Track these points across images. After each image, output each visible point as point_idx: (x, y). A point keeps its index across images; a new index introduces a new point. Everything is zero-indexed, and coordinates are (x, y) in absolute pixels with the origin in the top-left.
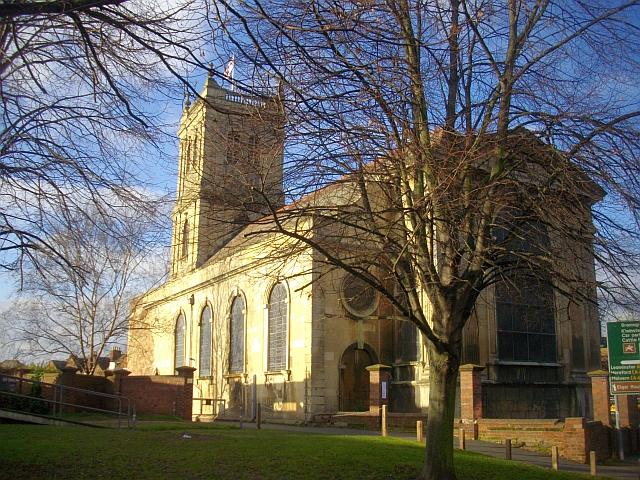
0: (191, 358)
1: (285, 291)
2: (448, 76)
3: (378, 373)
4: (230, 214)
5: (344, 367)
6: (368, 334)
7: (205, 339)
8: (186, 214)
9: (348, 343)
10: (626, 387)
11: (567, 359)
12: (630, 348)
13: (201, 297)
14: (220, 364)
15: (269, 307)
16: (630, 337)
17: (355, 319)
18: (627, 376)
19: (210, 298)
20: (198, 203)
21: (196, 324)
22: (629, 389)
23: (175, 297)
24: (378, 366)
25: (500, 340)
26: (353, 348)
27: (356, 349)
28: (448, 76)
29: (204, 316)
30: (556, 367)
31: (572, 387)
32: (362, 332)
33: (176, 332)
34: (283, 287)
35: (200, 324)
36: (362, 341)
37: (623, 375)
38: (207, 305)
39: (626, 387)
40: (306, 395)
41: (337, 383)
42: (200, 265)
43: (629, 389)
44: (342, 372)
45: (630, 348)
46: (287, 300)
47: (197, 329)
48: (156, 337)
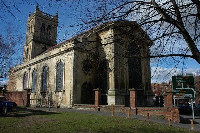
0: (29, 86)
1: (63, 64)
2: (176, 14)
3: (98, 91)
4: (42, 46)
5: (83, 89)
6: (90, 79)
7: (34, 81)
8: (28, 46)
9: (84, 82)
10: (178, 96)
11: (144, 89)
12: (179, 84)
13: (32, 67)
14: (144, 86)
15: (57, 70)
16: (179, 81)
17: (86, 74)
18: (178, 93)
19: (36, 67)
20: (32, 43)
21: (31, 75)
22: (179, 97)
23: (24, 68)
24: (98, 89)
25: (129, 82)
26: (85, 83)
27: (87, 83)
28: (176, 14)
29: (33, 73)
30: (142, 91)
31: (146, 96)
32: (88, 78)
33: (24, 78)
34: (62, 63)
35: (32, 76)
36: (88, 81)
37: (177, 93)
38: (35, 70)
39: (178, 96)
40: (70, 99)
41: (80, 95)
42: (33, 56)
43: (179, 97)
44: (82, 91)
45: (179, 84)
46: (64, 67)
47: (31, 78)
48: (17, 80)
